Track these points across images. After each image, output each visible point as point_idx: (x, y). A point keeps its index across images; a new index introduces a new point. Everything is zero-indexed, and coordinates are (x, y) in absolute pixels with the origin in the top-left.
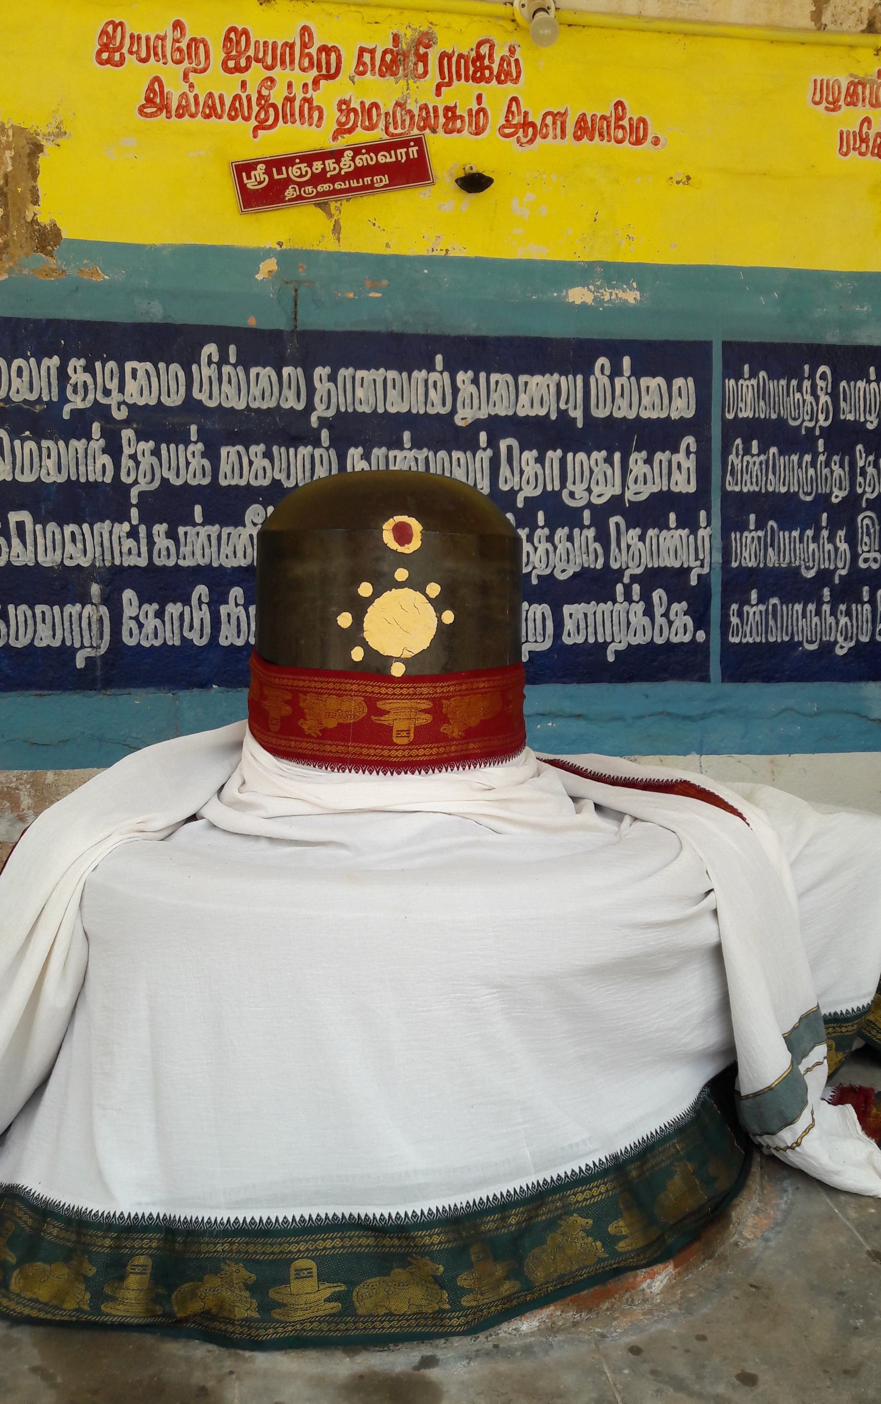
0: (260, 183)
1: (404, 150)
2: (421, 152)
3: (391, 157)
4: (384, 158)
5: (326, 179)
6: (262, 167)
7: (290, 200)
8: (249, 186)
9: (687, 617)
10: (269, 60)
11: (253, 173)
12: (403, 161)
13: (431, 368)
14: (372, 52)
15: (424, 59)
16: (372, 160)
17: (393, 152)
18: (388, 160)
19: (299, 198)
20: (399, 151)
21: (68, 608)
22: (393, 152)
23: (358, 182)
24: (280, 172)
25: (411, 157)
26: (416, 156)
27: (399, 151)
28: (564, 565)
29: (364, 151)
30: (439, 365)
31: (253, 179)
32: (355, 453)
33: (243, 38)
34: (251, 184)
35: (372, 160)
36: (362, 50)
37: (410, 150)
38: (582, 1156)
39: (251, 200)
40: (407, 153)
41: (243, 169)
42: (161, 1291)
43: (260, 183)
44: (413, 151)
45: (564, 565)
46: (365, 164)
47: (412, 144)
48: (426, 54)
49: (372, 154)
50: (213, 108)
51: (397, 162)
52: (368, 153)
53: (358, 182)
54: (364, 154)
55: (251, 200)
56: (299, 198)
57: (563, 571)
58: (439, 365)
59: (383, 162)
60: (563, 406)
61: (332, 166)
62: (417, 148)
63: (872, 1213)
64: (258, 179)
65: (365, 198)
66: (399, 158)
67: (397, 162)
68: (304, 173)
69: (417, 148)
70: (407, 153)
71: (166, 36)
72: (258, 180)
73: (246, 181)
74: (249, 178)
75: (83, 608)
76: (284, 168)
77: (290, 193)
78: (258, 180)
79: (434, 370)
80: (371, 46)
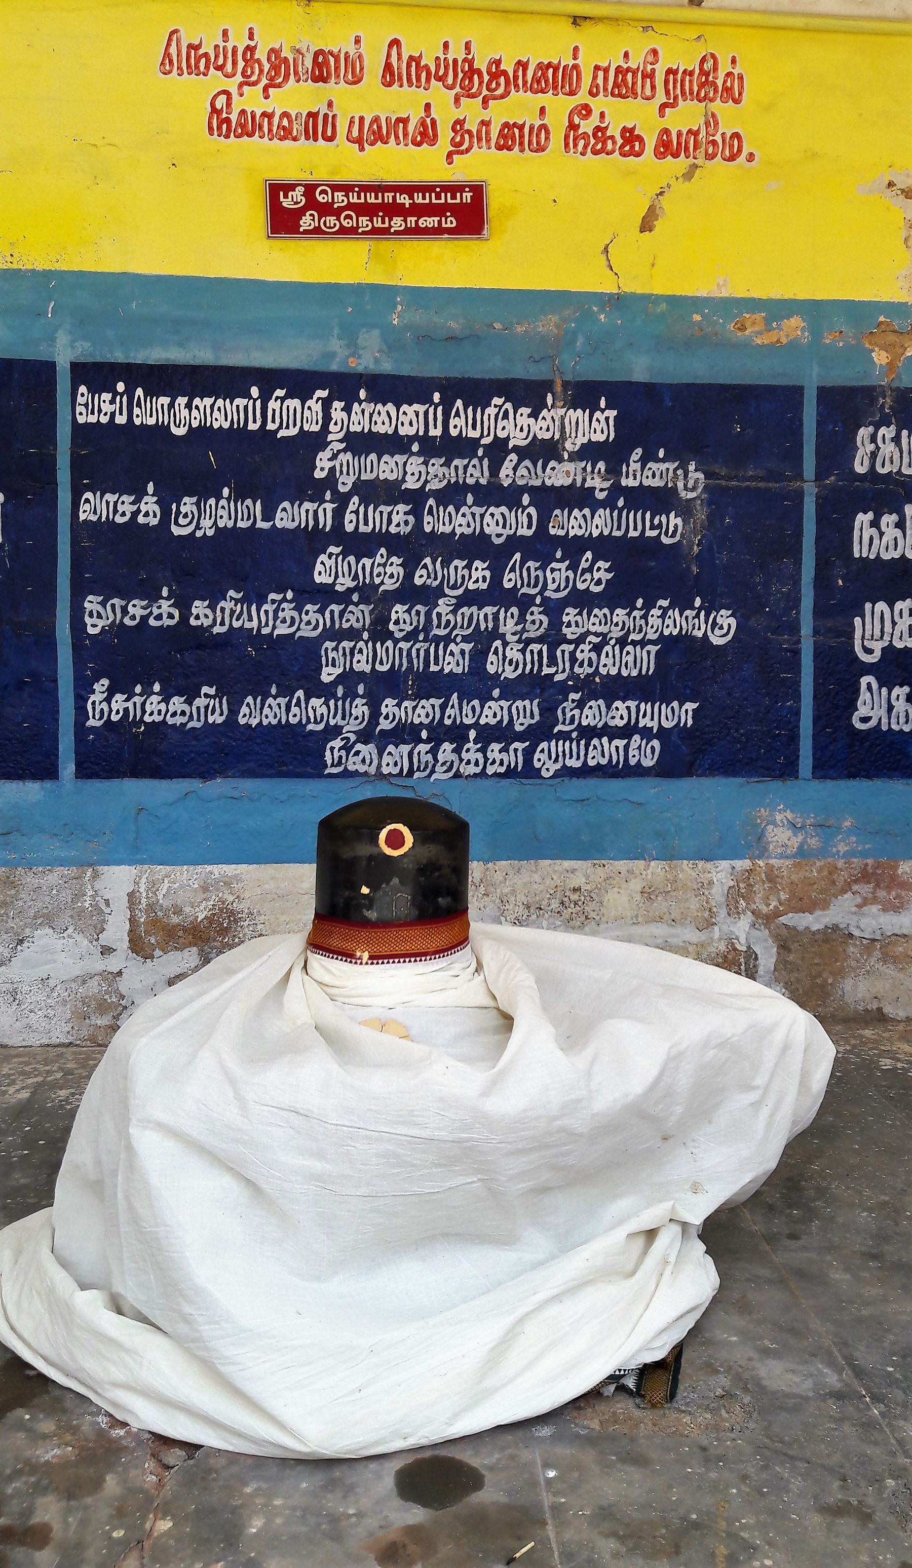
5: (384, 210)
6: (300, 190)
7: (306, 232)
10: (450, 80)
11: (290, 194)
14: (606, 70)
15: (652, 76)
19: (317, 231)
26: (469, 201)
27: (386, 194)
31: (290, 199)
32: (199, 607)
33: (203, 60)
34: (286, 203)
36: (597, 68)
37: (464, 195)
39: (282, 222)
41: (276, 189)
42: (630, 1383)
44: (467, 196)
48: (653, 71)
50: (243, 126)
55: (282, 222)
56: (317, 231)
60: (646, 754)
61: (341, 198)
65: (409, 244)
71: (524, 124)
74: (286, 197)
80: (605, 64)
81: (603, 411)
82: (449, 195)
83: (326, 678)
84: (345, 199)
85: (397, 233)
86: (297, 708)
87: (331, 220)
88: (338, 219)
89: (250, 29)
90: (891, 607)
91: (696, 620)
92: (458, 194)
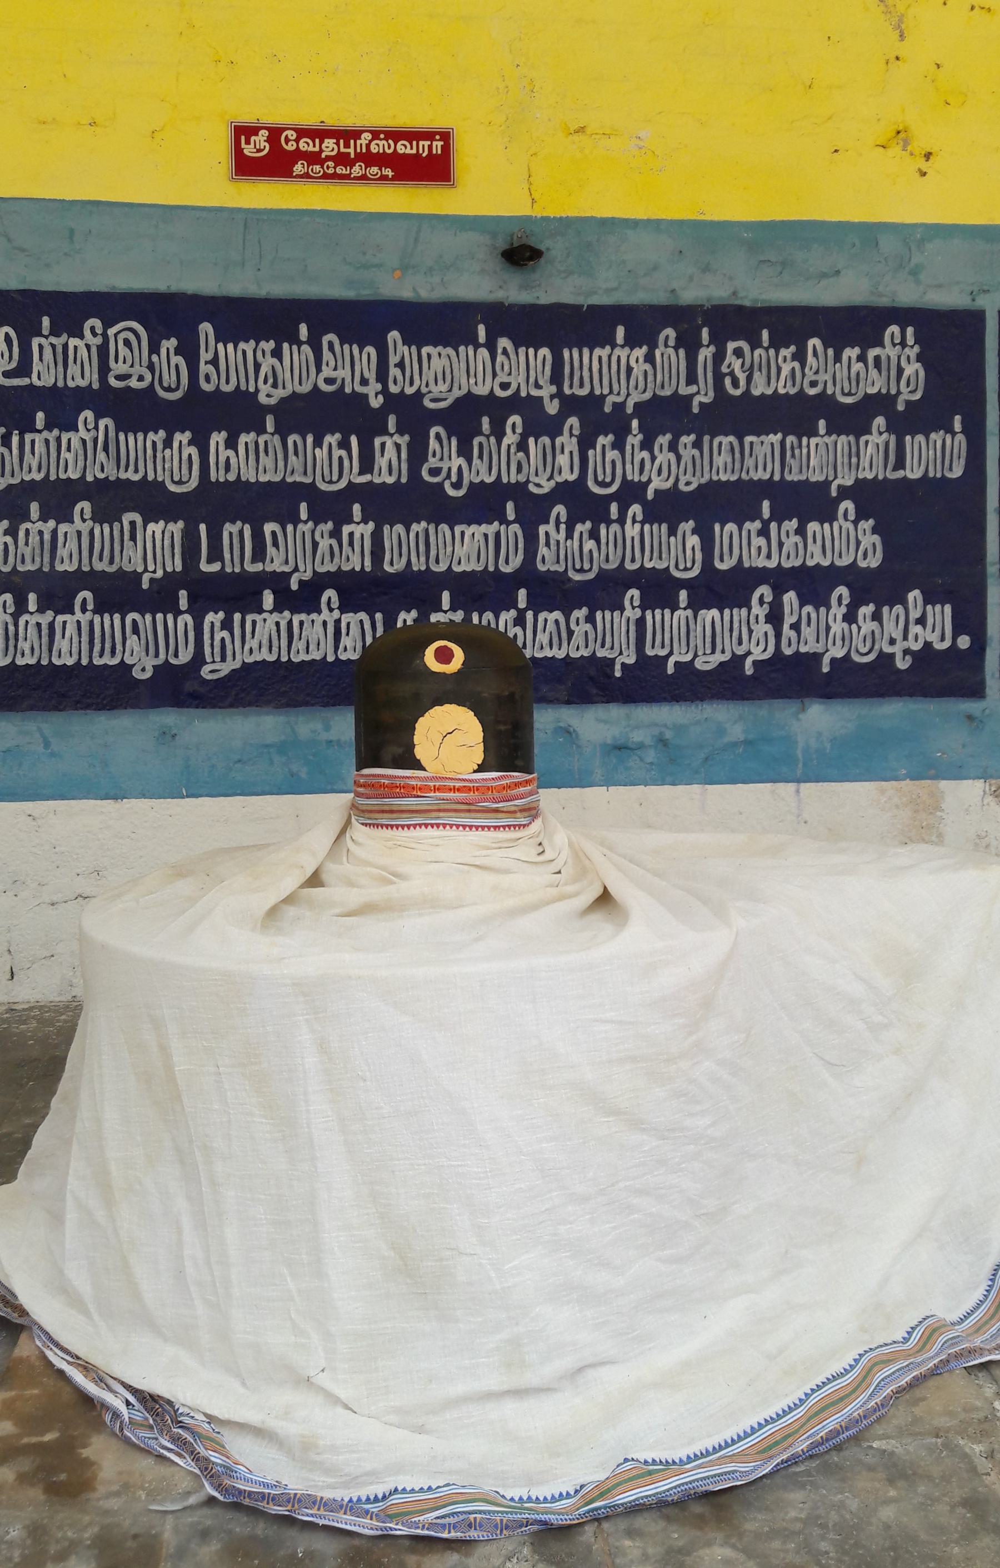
0: (259, 151)
1: (427, 143)
2: (446, 148)
3: (412, 148)
4: (403, 148)
6: (264, 134)
8: (246, 152)
9: (760, 538)
11: (253, 138)
12: (424, 155)
13: (261, 430)
16: (389, 148)
17: (414, 143)
18: (408, 151)
19: (364, 177)
20: (421, 143)
21: (598, 352)
22: (414, 143)
24: (347, 145)
25: (434, 152)
26: (439, 152)
27: (421, 143)
28: (689, 477)
29: (382, 136)
30: (270, 427)
31: (252, 145)
34: (248, 150)
35: (389, 148)
37: (435, 143)
39: (245, 167)
40: (430, 147)
41: (243, 132)
43: (259, 151)
44: (438, 145)
45: (689, 477)
46: (381, 151)
47: (438, 137)
49: (390, 142)
51: (418, 155)
52: (386, 139)
54: (381, 140)
56: (306, 176)
57: (688, 484)
58: (270, 427)
59: (401, 152)
64: (258, 146)
65: (260, 185)
66: (421, 151)
67: (418, 155)
70: (430, 147)
73: (243, 145)
75: (612, 350)
76: (352, 142)
77: (299, 168)
79: (265, 432)
81: (46, 337)
82: (342, 142)
83: (573, 421)
84: (335, 147)
85: (356, 178)
86: (861, 365)
87: (317, 168)
88: (322, 167)
89: (902, 40)
90: (403, 390)
91: (168, 451)
92: (352, 142)
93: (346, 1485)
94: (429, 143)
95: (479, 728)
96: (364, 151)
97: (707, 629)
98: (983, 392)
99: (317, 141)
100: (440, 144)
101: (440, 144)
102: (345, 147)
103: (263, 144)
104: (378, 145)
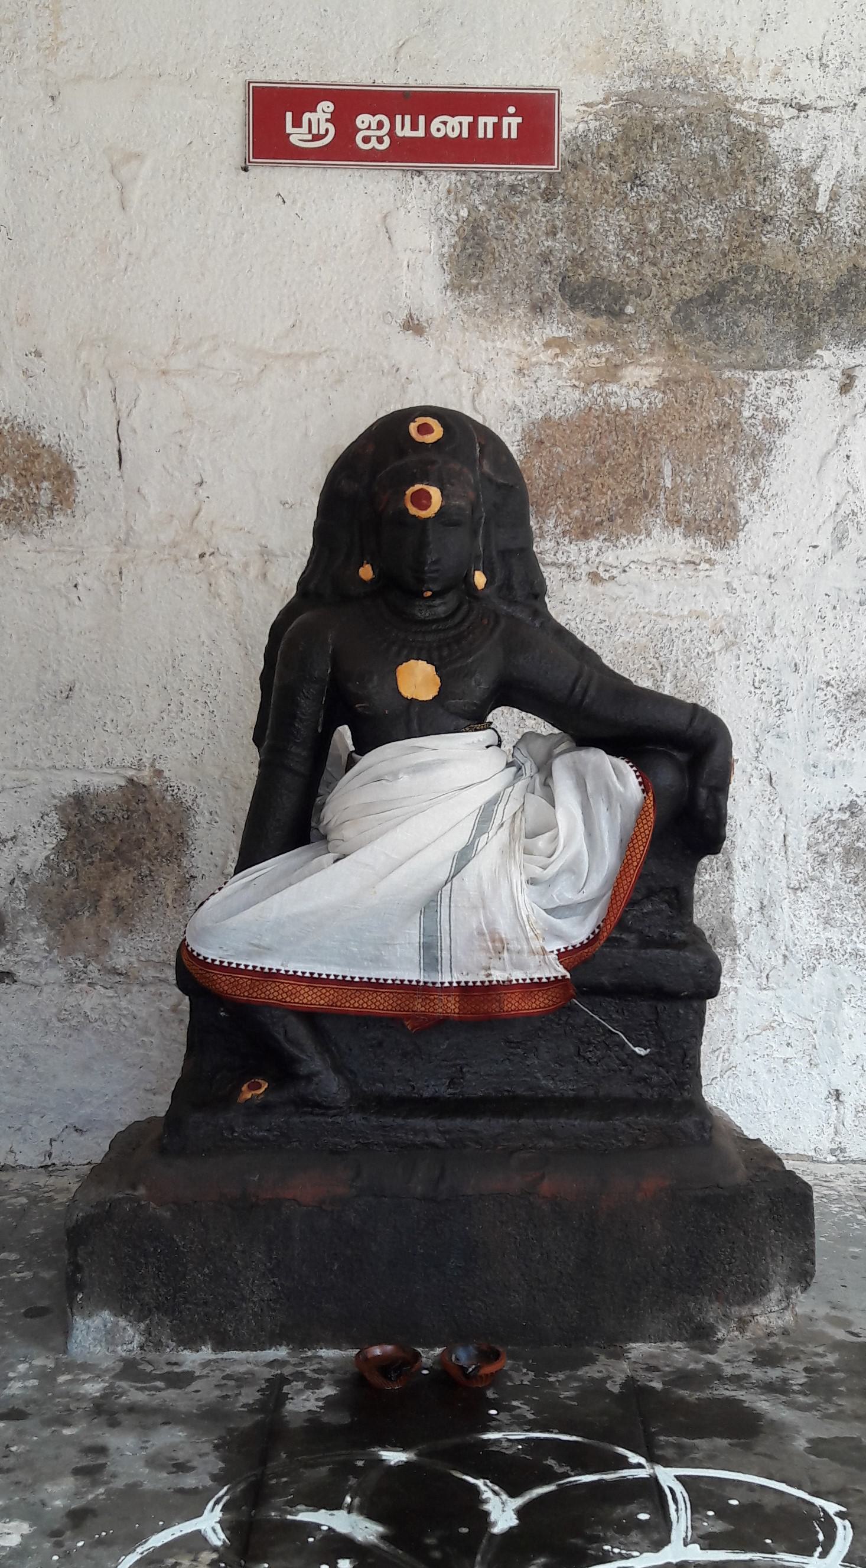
0: (317, 137)
1: (491, 120)
6: (326, 107)
11: (306, 116)
23: (414, 127)
26: (514, 135)
37: (506, 120)
38: (321, 962)
40: (497, 127)
43: (317, 137)
47: (512, 110)
53: (414, 127)
62: (519, 120)
63: (464, 1534)
68: (322, 132)
69: (519, 120)
70: (497, 127)
72: (315, 131)
74: (297, 124)
78: (315, 131)
93: (249, 955)
94: (495, 119)
95: (425, 699)
96: (490, 135)
97: (403, 870)
98: (736, 1561)
99: (422, 119)
100: (516, 121)
101: (516, 121)
102: (293, 126)
103: (324, 126)
104: (445, 123)
